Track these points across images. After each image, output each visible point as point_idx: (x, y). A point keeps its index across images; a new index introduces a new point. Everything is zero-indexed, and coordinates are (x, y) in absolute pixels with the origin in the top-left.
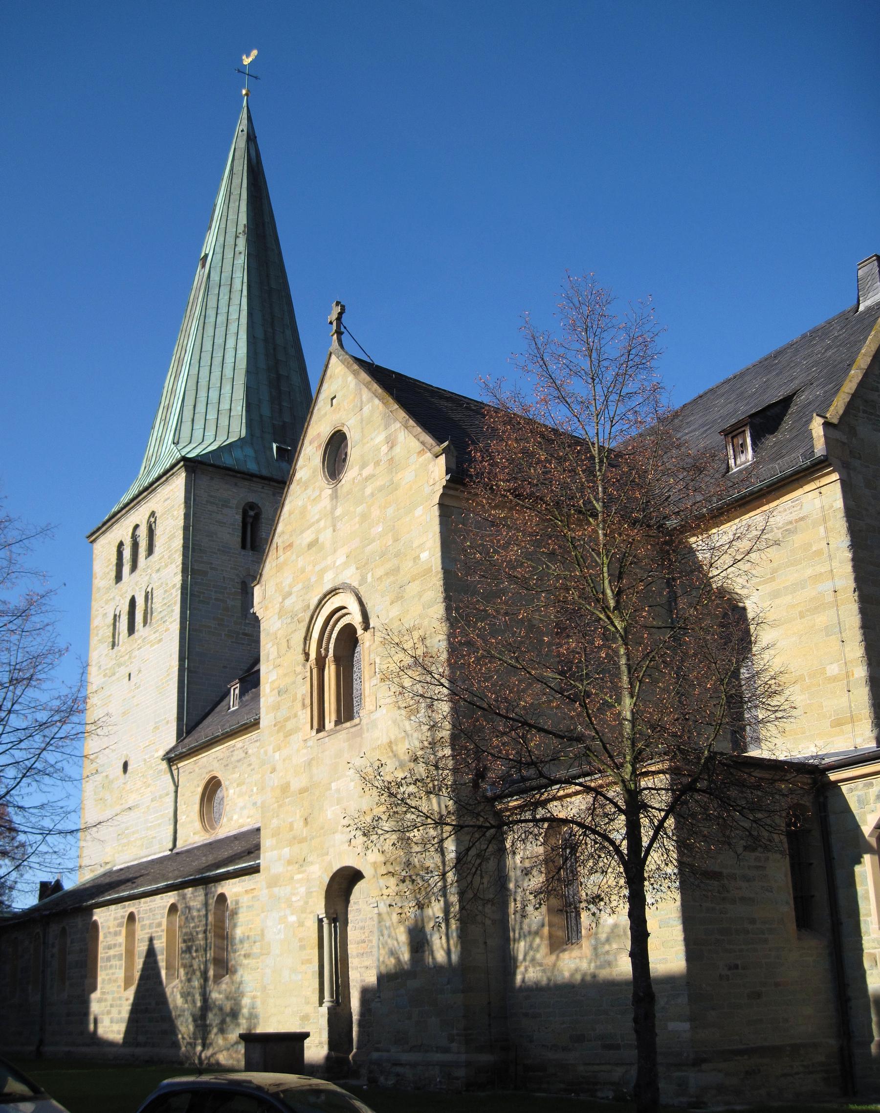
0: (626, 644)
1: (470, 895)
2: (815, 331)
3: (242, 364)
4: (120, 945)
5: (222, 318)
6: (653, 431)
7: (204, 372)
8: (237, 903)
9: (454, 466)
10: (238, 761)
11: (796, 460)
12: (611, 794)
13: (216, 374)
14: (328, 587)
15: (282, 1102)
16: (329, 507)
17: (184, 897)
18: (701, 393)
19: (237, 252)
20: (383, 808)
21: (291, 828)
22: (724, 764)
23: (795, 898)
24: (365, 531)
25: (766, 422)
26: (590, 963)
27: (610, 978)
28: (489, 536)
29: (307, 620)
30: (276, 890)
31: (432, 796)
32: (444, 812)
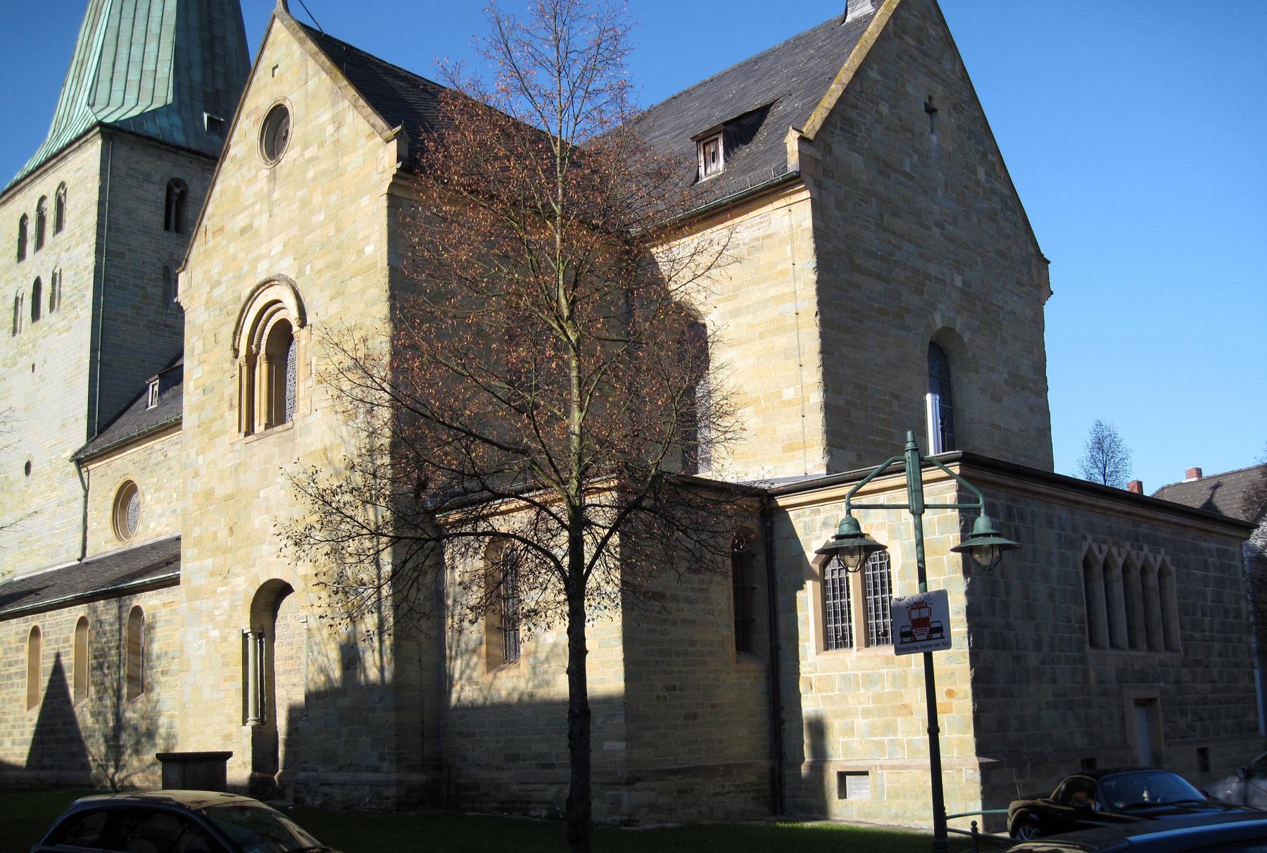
0: (578, 356)
1: (405, 606)
2: (799, 38)
3: (171, 20)
4: (22, 661)
6: (618, 133)
7: (126, 25)
8: (154, 616)
9: (406, 154)
10: (157, 464)
11: (767, 174)
12: (554, 510)
13: (140, 28)
14: (262, 277)
15: (205, 819)
16: (265, 189)
17: (95, 611)
18: (676, 94)
20: (316, 517)
21: (215, 539)
22: (671, 484)
23: (736, 621)
24: (305, 216)
25: (740, 130)
26: (527, 682)
27: (546, 697)
28: (439, 232)
29: (238, 313)
30: (197, 603)
31: (368, 506)
32: (380, 522)
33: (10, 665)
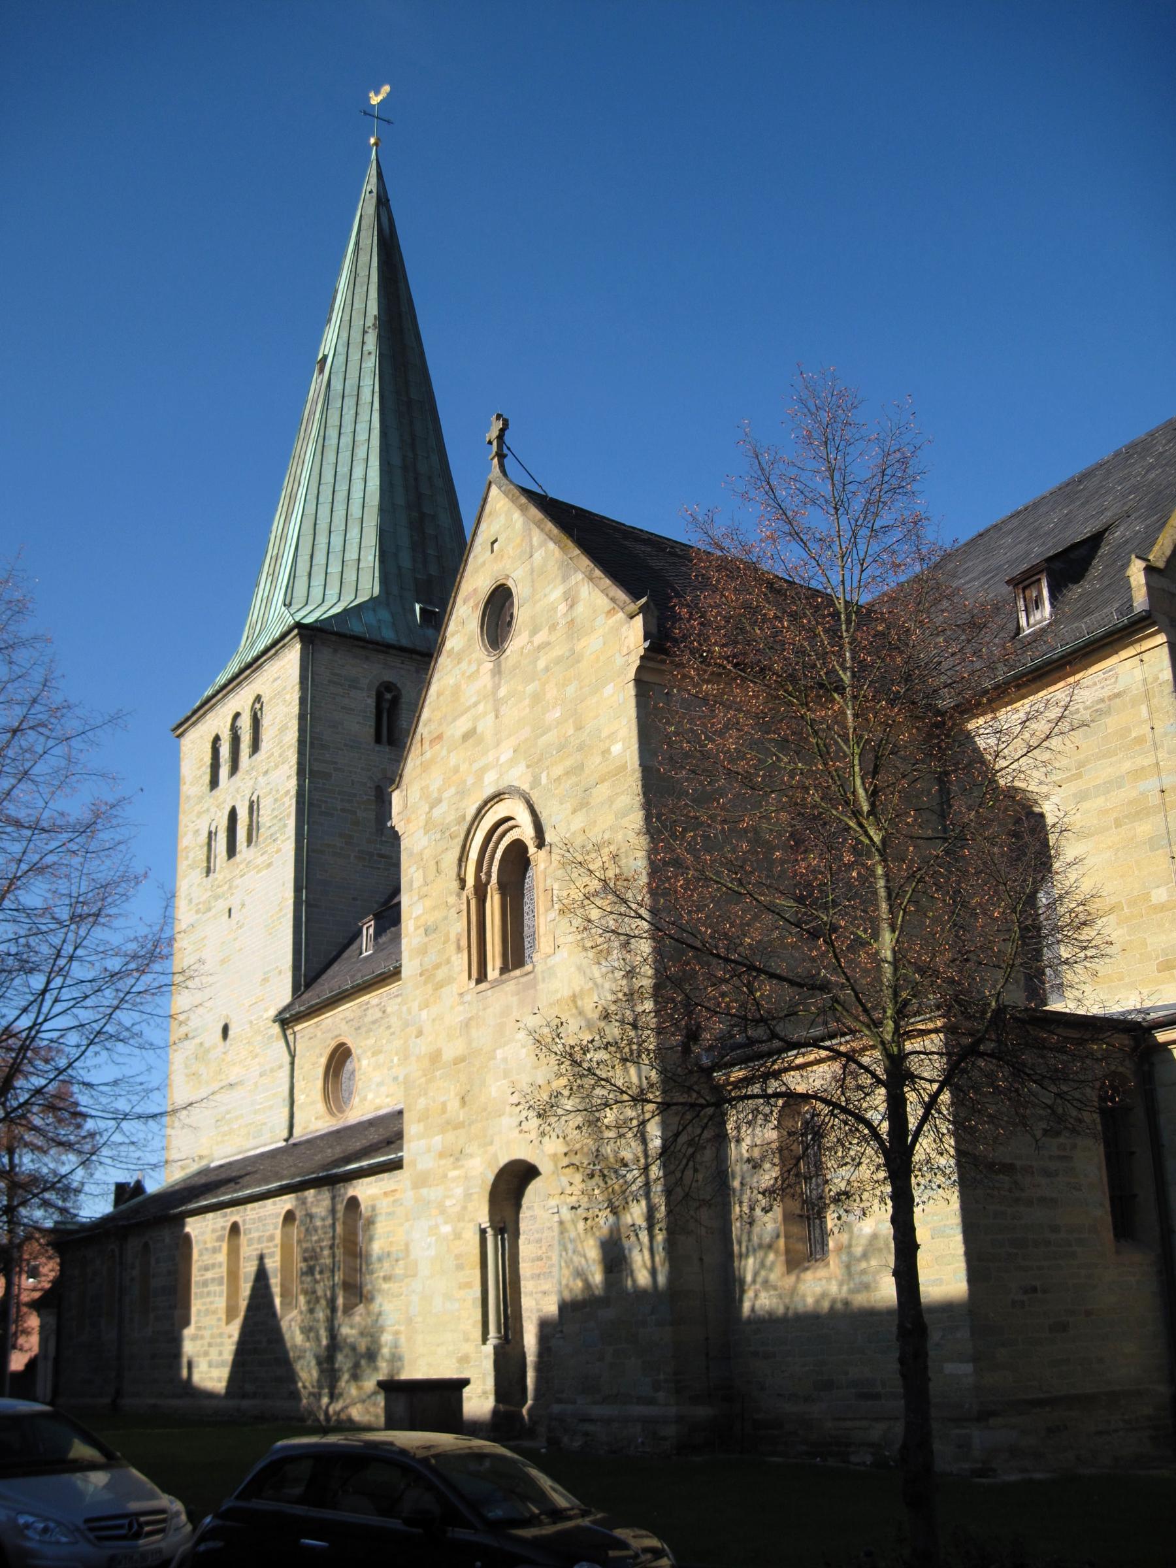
5: (346, 440)
14: (489, 791)
19: (365, 353)
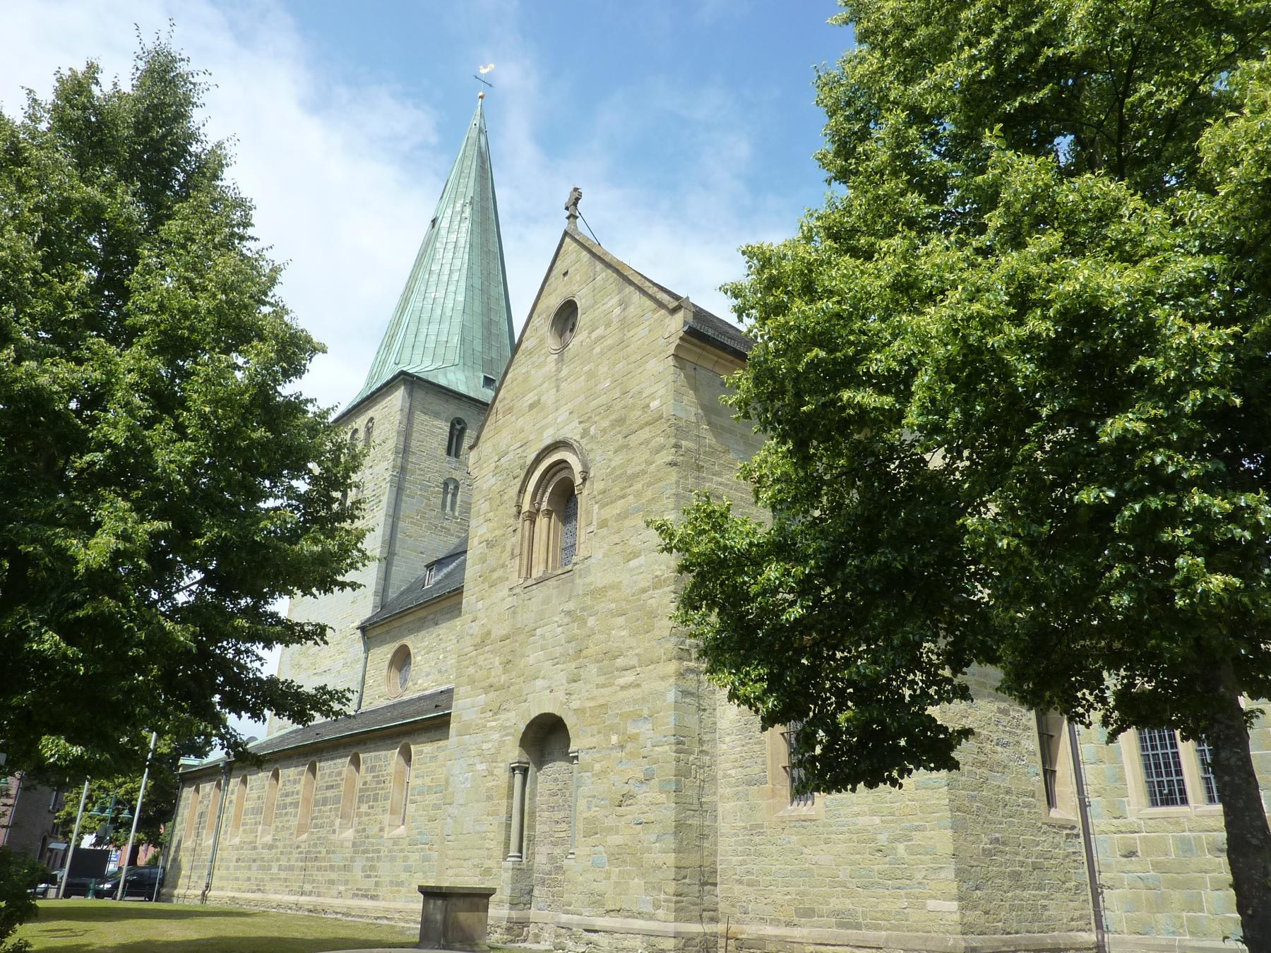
14: (548, 441)
33: (287, 795)
